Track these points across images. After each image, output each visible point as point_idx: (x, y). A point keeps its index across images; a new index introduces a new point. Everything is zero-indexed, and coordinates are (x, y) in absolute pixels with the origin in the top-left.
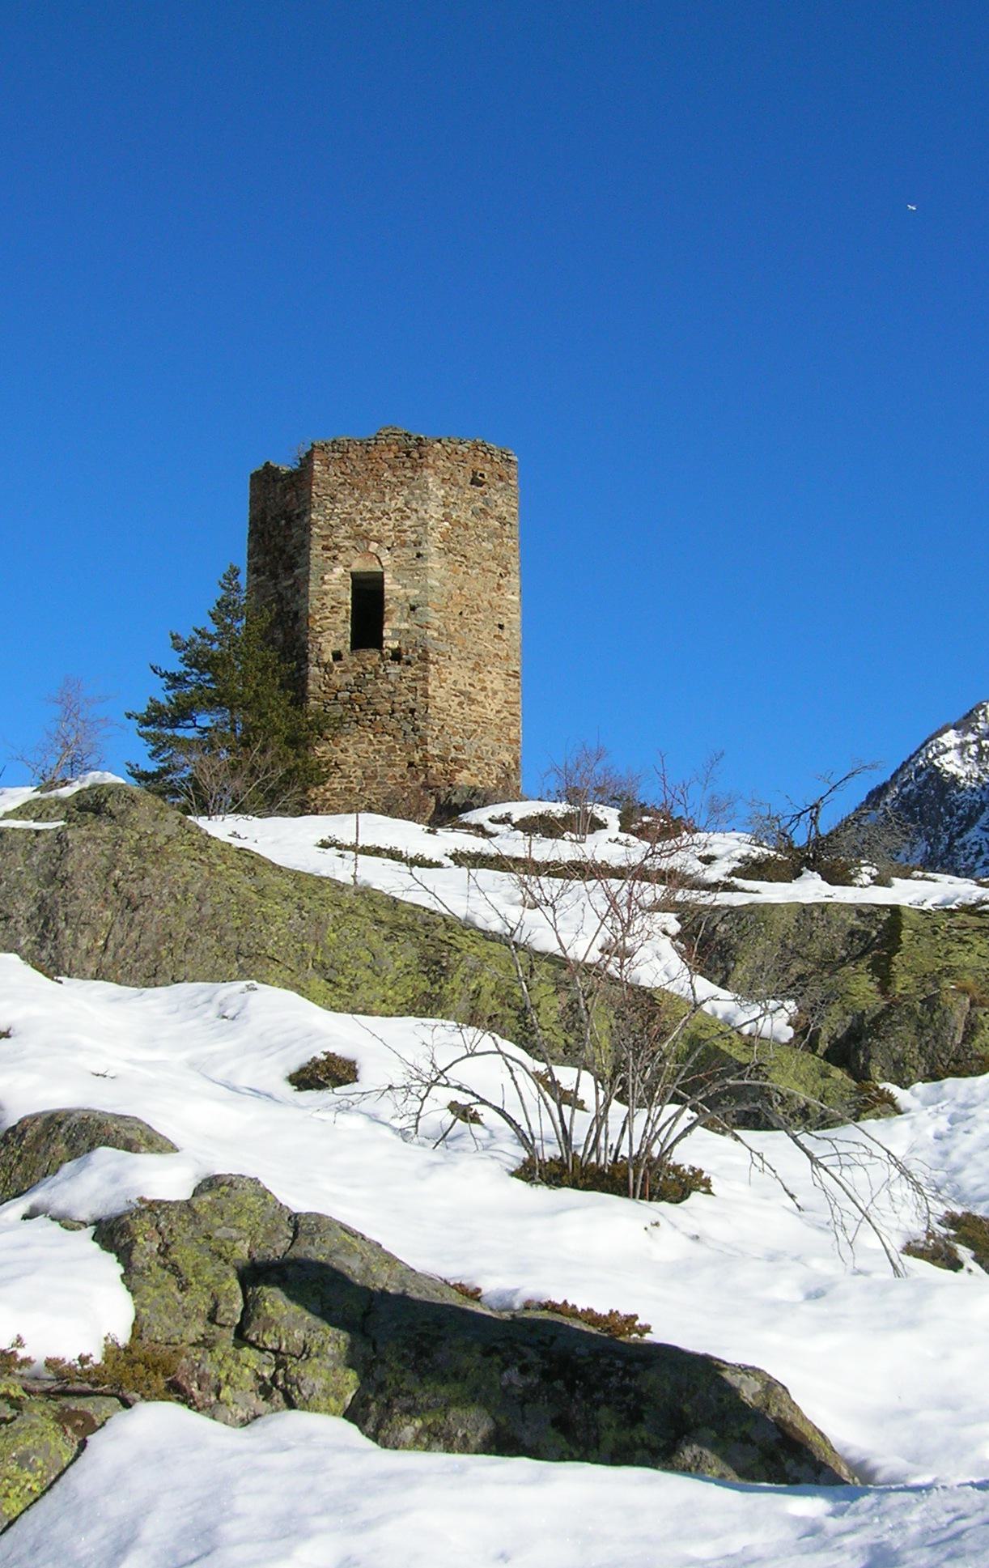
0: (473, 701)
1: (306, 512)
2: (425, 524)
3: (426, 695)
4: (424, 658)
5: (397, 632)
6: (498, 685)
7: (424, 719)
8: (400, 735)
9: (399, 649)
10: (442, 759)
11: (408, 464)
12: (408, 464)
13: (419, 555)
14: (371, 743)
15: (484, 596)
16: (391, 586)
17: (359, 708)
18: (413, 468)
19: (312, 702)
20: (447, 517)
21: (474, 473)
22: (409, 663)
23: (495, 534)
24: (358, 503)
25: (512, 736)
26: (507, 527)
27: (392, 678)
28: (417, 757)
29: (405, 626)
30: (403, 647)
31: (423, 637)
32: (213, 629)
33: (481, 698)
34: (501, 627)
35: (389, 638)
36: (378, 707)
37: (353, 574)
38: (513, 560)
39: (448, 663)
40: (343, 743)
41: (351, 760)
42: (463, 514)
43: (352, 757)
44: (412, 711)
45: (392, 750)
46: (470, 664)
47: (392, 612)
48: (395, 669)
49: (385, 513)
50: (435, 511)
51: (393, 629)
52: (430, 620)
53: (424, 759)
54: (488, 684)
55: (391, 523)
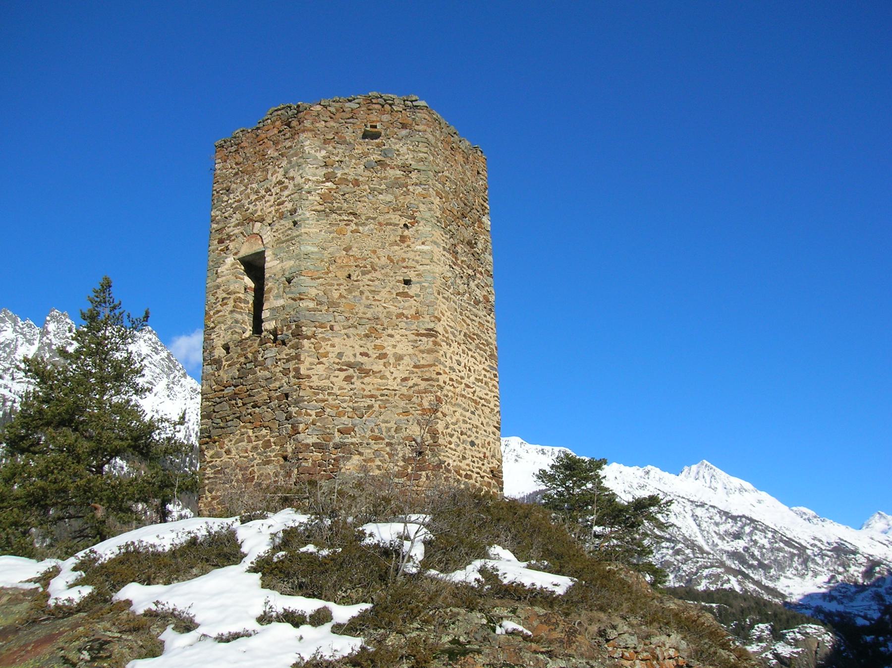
0: (367, 373)
3: (298, 376)
4: (298, 334)
5: (272, 309)
6: (404, 348)
7: (296, 403)
16: (271, 264)
20: (328, 178)
24: (247, 188)
25: (426, 405)
26: (414, 175)
27: (269, 363)
28: (289, 449)
29: (280, 302)
30: (279, 326)
31: (297, 310)
33: (378, 366)
35: (268, 320)
38: (422, 207)
40: (227, 444)
42: (353, 170)
44: (287, 396)
45: (267, 444)
46: (362, 331)
48: (272, 352)
50: (312, 173)
52: (303, 289)
53: (296, 451)
54: (389, 351)
55: (272, 199)
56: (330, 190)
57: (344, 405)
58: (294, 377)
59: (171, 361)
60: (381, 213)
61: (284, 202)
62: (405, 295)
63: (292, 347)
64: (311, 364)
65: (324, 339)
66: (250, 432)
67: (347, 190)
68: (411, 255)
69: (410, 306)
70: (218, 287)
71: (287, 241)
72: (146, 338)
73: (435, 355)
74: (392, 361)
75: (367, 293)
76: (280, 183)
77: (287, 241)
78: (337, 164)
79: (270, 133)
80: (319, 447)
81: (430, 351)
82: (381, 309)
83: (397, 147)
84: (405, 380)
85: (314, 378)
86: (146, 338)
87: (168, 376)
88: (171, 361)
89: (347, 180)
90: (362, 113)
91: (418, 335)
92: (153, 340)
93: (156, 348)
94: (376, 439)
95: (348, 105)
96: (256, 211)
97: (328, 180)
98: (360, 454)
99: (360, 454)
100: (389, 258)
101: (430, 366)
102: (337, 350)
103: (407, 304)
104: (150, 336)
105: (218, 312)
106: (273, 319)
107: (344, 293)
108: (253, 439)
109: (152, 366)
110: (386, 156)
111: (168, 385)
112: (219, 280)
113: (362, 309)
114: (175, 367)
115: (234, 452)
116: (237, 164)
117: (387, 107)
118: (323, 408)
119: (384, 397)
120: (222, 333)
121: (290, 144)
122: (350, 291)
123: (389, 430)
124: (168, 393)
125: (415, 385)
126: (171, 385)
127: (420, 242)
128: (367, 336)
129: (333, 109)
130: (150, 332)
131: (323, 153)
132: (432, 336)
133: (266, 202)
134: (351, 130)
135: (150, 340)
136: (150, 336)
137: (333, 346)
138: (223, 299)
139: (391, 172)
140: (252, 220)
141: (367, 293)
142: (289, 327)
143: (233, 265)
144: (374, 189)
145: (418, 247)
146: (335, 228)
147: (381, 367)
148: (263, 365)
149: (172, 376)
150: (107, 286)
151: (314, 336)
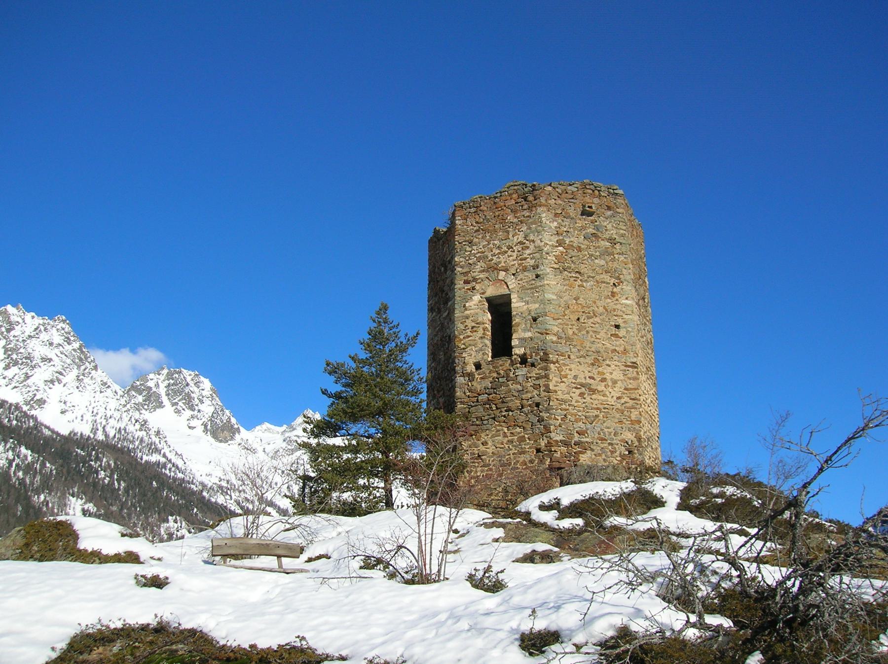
0: (593, 391)
1: (453, 258)
2: (540, 250)
3: (548, 390)
4: (545, 359)
6: (617, 375)
7: (547, 410)
8: (529, 426)
9: (525, 354)
10: (566, 444)
11: (526, 207)
12: (526, 207)
13: (537, 276)
14: (505, 435)
15: (599, 303)
16: (517, 305)
17: (495, 405)
18: (530, 209)
19: (459, 406)
20: (560, 243)
21: (584, 206)
22: (533, 365)
23: (606, 253)
25: (633, 417)
26: (618, 246)
27: (520, 379)
28: (543, 443)
29: (528, 335)
30: (528, 352)
31: (544, 342)
32: (363, 355)
33: (601, 387)
34: (617, 327)
35: (517, 346)
36: (510, 404)
37: (489, 300)
38: (625, 272)
39: (567, 361)
41: (490, 451)
42: (576, 239)
43: (491, 449)
44: (538, 405)
45: (522, 439)
46: (589, 360)
47: (518, 325)
48: (522, 371)
49: (510, 247)
50: (548, 239)
51: (521, 338)
52: (548, 327)
54: (608, 376)
55: (515, 254)
56: (562, 253)
57: (580, 414)
58: (544, 391)
59: (82, 352)
60: (597, 273)
61: (525, 259)
62: (616, 336)
63: (541, 369)
64: (557, 382)
65: (565, 365)
66: (506, 430)
67: (573, 254)
68: (618, 307)
69: (619, 345)
70: (467, 318)
71: (531, 289)
72: (59, 327)
73: (636, 381)
74: (610, 384)
75: (591, 333)
76: (521, 243)
77: (531, 289)
78: (565, 234)
79: (508, 203)
80: (566, 444)
81: (635, 379)
82: (600, 345)
83: (605, 224)
84: (618, 398)
85: (559, 393)
86: (59, 327)
87: (79, 367)
88: (82, 352)
89: (572, 246)
90: (579, 195)
91: (626, 366)
92: (66, 330)
93: (68, 338)
94: (602, 439)
95: (569, 188)
96: (500, 262)
97: (560, 245)
98: (592, 450)
99: (592, 450)
100: (604, 307)
101: (635, 389)
102: (573, 373)
103: (618, 343)
104: (64, 326)
105: (469, 337)
106: (522, 347)
107: (576, 332)
108: (508, 434)
109: (63, 356)
110: (598, 230)
111: (78, 376)
112: (467, 312)
113: (588, 345)
114: (86, 358)
115: (490, 443)
116: (477, 223)
117: (596, 192)
118: (565, 415)
119: (606, 409)
120: (474, 354)
121: (528, 214)
122: (580, 330)
123: (610, 433)
124: (77, 384)
125: (626, 402)
126: (81, 377)
127: (624, 297)
128: (593, 364)
129: (560, 191)
130: (64, 321)
131: (555, 224)
132: (636, 367)
133: (509, 256)
134: (573, 208)
135: (63, 329)
136: (64, 326)
137: (570, 370)
138: (473, 328)
139: (602, 242)
140: (496, 269)
141: (591, 333)
142: (537, 354)
143: (480, 301)
144: (592, 255)
145: (624, 301)
146: (567, 282)
147: (603, 388)
148: (515, 380)
149: (83, 368)
150: (385, 308)
151: (557, 362)
